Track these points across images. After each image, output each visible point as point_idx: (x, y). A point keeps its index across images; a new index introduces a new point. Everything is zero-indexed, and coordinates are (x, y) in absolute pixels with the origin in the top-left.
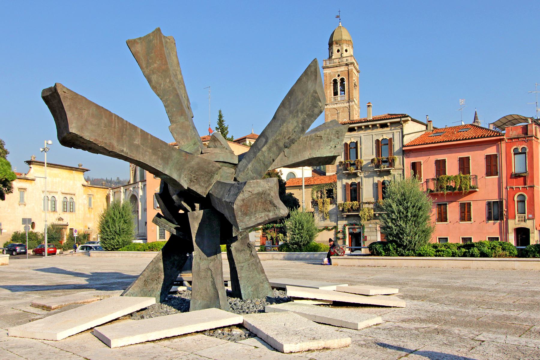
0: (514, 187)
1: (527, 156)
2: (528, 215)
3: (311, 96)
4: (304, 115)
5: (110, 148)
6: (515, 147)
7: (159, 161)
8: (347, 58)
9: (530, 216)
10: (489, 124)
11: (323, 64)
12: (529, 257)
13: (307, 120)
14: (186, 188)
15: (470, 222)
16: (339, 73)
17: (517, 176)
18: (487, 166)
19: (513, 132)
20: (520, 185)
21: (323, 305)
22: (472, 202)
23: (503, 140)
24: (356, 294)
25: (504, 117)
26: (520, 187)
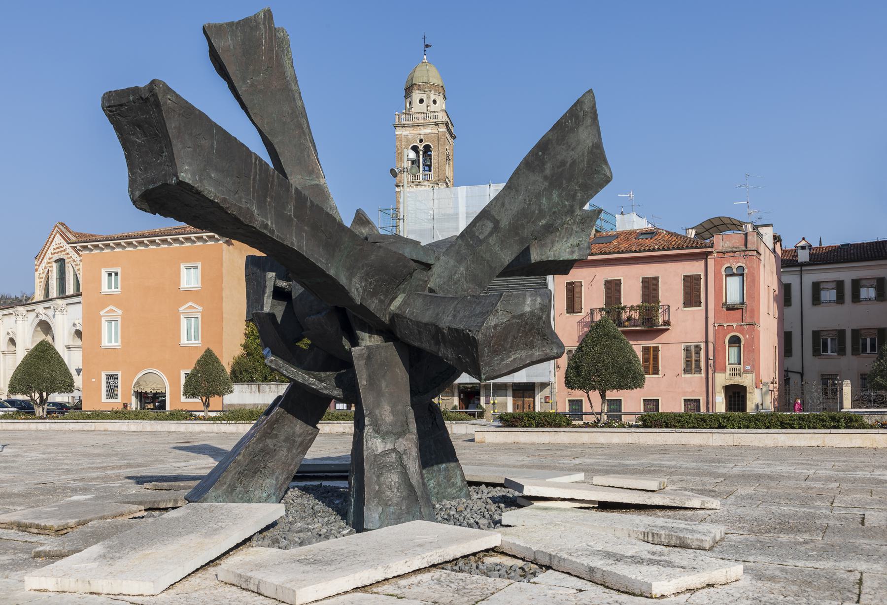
0: (725, 325)
1: (745, 279)
2: (744, 367)
3: (588, 153)
4: (573, 184)
5: (246, 218)
6: (728, 265)
7: (321, 250)
8: (436, 114)
9: (748, 368)
10: (686, 229)
11: (395, 120)
12: (516, 426)
13: (579, 194)
14: (359, 303)
15: (699, 375)
16: (422, 137)
17: (731, 308)
18: (568, 298)
19: (725, 243)
20: (734, 322)
21: (581, 508)
22: (660, 345)
23: (711, 253)
24: (630, 489)
25: (710, 220)
26: (734, 324)
